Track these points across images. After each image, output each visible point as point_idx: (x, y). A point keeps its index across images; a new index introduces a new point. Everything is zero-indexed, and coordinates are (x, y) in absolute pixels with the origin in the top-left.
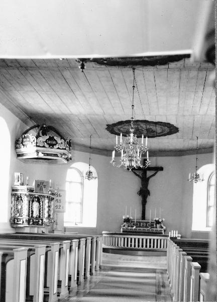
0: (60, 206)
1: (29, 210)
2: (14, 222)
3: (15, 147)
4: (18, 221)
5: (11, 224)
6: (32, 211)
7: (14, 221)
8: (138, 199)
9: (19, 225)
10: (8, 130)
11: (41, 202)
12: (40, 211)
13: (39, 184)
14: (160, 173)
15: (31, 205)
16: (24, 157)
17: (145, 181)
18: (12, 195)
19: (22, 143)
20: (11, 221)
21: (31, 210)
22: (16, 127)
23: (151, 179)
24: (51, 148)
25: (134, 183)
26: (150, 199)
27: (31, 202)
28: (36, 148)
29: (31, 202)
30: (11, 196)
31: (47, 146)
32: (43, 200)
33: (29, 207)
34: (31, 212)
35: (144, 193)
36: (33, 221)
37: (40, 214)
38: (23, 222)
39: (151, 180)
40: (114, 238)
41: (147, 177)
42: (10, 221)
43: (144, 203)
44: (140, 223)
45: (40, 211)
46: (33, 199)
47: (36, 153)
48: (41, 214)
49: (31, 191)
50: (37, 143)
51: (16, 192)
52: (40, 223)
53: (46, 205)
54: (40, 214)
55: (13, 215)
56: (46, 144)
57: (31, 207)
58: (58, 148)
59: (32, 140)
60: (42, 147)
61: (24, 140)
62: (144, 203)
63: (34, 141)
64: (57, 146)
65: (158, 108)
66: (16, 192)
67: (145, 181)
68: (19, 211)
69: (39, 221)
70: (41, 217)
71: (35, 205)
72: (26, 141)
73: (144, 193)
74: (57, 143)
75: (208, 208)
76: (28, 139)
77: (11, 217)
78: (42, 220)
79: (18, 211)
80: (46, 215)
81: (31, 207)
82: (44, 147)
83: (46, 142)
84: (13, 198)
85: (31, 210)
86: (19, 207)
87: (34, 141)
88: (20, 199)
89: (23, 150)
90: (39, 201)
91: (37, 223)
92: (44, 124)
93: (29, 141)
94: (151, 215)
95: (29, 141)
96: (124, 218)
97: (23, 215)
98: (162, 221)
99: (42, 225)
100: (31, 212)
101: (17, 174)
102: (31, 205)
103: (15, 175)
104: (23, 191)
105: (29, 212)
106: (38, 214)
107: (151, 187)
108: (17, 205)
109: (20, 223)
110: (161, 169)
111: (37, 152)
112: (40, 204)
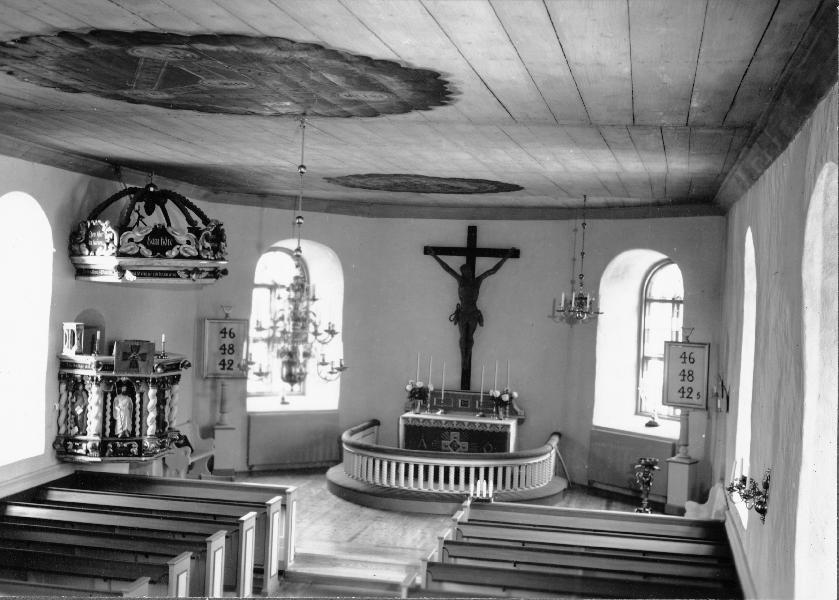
0: (232, 362)
1: (104, 416)
2: (64, 447)
3: (70, 248)
4: (75, 447)
5: (59, 453)
6: (113, 422)
7: (65, 445)
8: (453, 333)
9: (79, 458)
10: (46, 220)
11: (137, 396)
12: (134, 419)
13: (129, 351)
14: (510, 262)
15: (109, 404)
16: (93, 279)
17: (469, 284)
18: (59, 375)
19: (86, 241)
20: (58, 446)
21: (109, 417)
22: (73, 199)
23: (485, 282)
24: (159, 257)
25: (445, 293)
26: (480, 335)
27: (109, 396)
28: (116, 261)
29: (109, 396)
30: (57, 382)
31: (147, 252)
32: (142, 389)
33: (105, 410)
34: (108, 423)
35: (468, 318)
36: (114, 446)
37: (134, 426)
38: (87, 451)
39: (486, 286)
40: (371, 461)
41: (478, 273)
42: (54, 447)
43: (467, 345)
44: (456, 397)
45: (134, 419)
46: (113, 388)
47: (116, 274)
48: (138, 426)
49: (107, 367)
50: (119, 246)
51: (70, 371)
52: (135, 450)
53: (152, 402)
54: (134, 426)
55: (62, 431)
56: (143, 247)
57: (109, 410)
58: (179, 257)
59: (108, 237)
60: (135, 256)
61: (93, 235)
62: (467, 345)
63: (112, 240)
64: (174, 253)
65: (301, 286)
66: (70, 371)
67: (469, 284)
68: (81, 423)
69: (130, 446)
70: (138, 433)
71: (122, 403)
72: (95, 238)
73: (468, 318)
74: (175, 243)
75: (642, 361)
76: (99, 234)
77: (58, 437)
78: (140, 442)
79: (76, 419)
80: (151, 429)
81: (109, 410)
82: (139, 255)
83: (144, 242)
84: (63, 386)
85: (109, 417)
86: (79, 410)
87: (112, 240)
88: (81, 387)
89: (89, 260)
90: (131, 394)
91: (127, 452)
92: (152, 185)
93: (103, 239)
94: (481, 381)
95: (103, 239)
96: (409, 388)
97: (87, 429)
98: (511, 398)
99: (140, 455)
100: (108, 419)
101: (70, 326)
102: (109, 404)
103: (65, 328)
104: (87, 366)
105: (104, 423)
106: (128, 427)
107: (485, 301)
108: (73, 403)
109: (79, 451)
110: (515, 253)
111: (121, 270)
112: (134, 400)
